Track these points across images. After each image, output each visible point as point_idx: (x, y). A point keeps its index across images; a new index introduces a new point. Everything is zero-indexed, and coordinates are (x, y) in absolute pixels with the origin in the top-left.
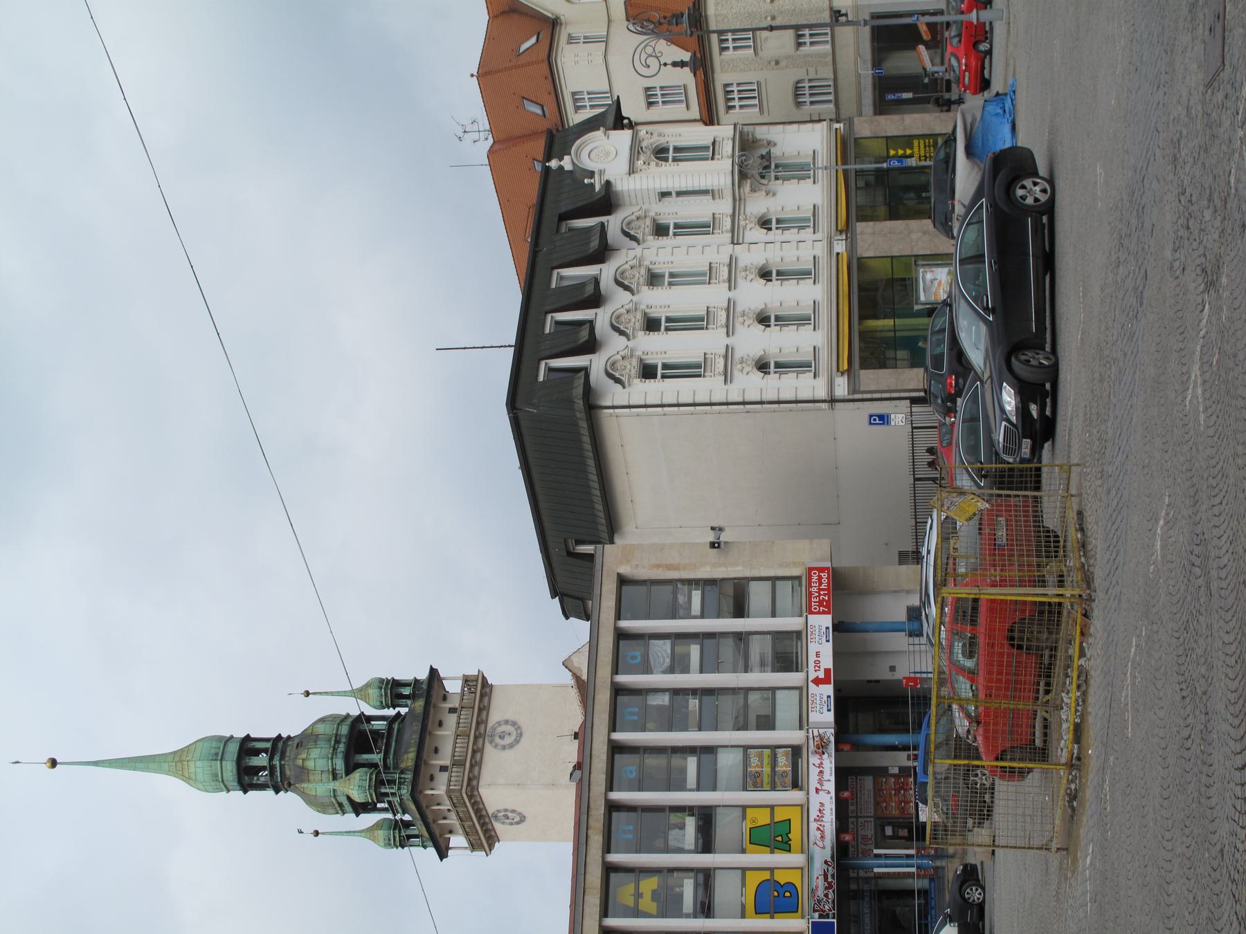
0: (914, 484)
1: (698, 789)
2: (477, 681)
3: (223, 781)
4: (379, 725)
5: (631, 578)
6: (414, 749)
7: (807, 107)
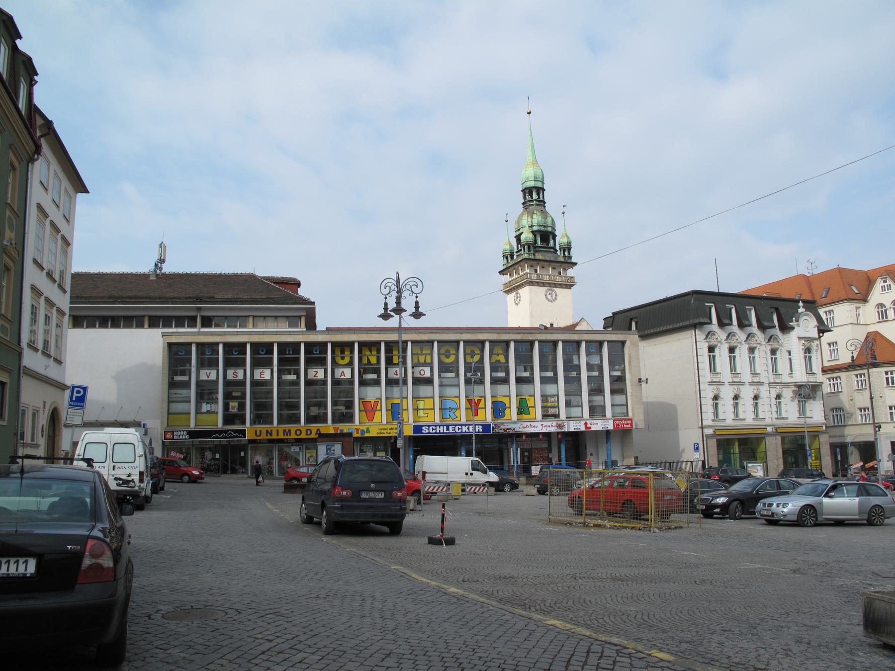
3: (526, 182)
4: (552, 243)
7: (831, 414)
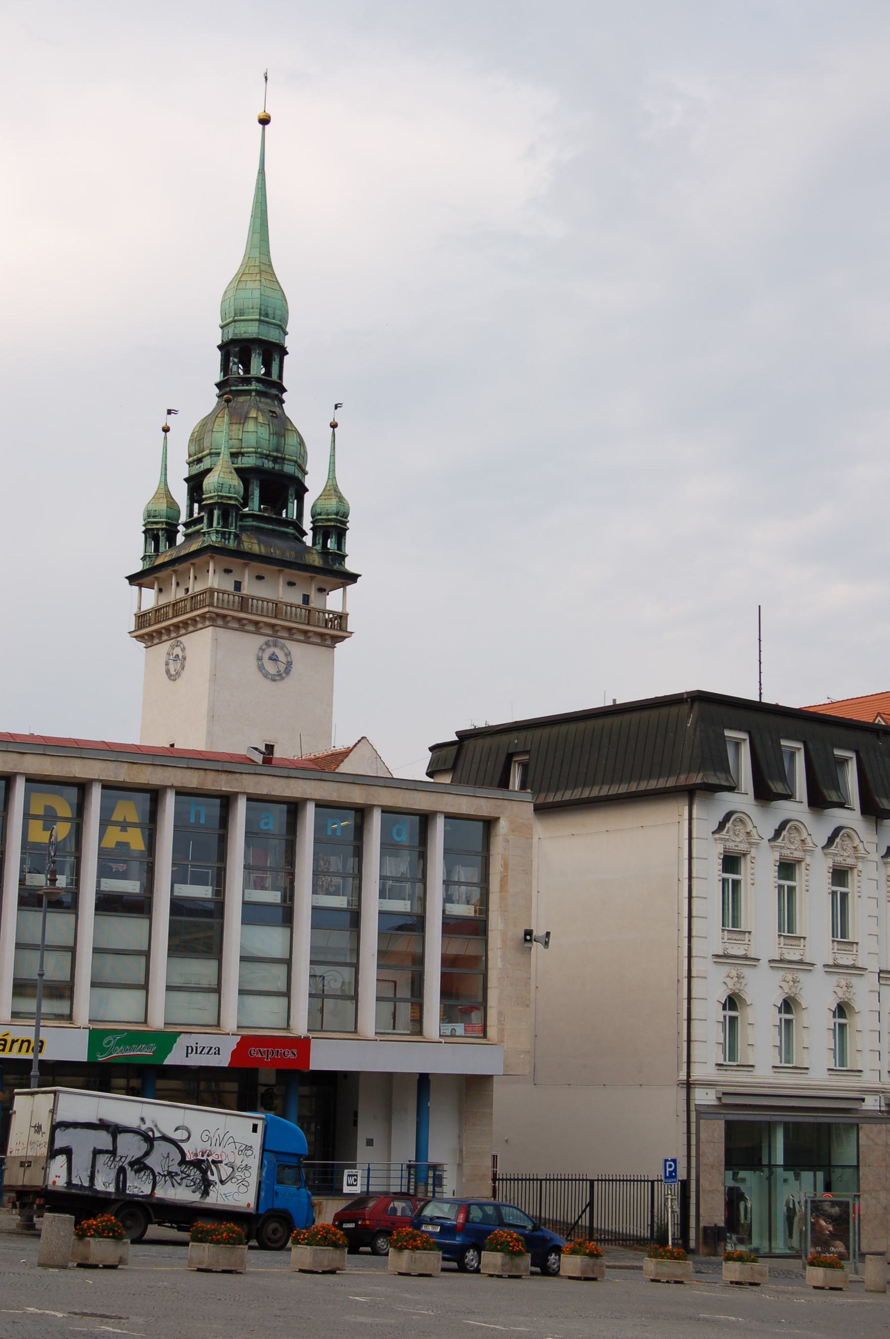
0: (586, 1180)
1: (245, 903)
2: (341, 629)
3: (235, 321)
5: (493, 834)
6: (263, 551)
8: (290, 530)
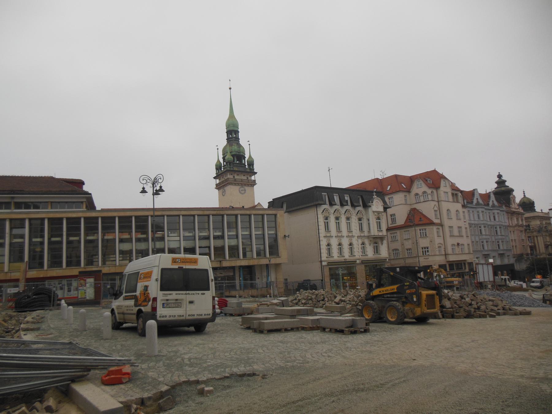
1: (228, 235)
6: (238, 170)
8: (243, 165)
